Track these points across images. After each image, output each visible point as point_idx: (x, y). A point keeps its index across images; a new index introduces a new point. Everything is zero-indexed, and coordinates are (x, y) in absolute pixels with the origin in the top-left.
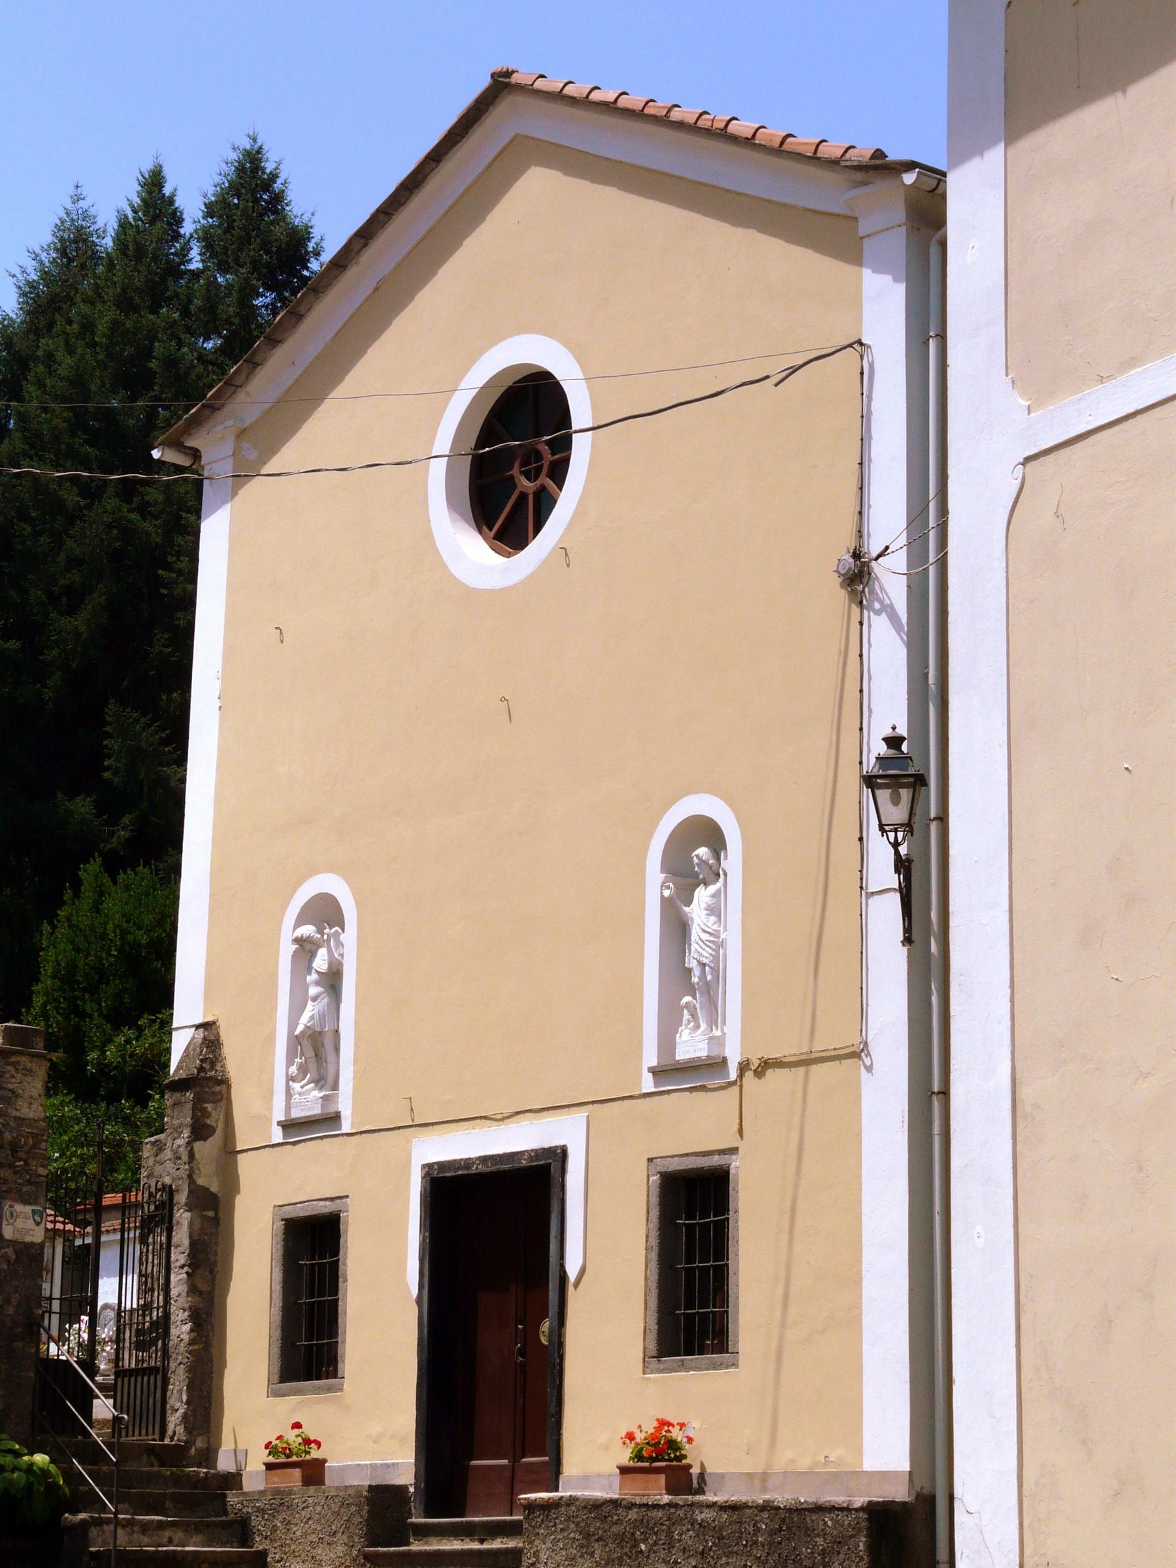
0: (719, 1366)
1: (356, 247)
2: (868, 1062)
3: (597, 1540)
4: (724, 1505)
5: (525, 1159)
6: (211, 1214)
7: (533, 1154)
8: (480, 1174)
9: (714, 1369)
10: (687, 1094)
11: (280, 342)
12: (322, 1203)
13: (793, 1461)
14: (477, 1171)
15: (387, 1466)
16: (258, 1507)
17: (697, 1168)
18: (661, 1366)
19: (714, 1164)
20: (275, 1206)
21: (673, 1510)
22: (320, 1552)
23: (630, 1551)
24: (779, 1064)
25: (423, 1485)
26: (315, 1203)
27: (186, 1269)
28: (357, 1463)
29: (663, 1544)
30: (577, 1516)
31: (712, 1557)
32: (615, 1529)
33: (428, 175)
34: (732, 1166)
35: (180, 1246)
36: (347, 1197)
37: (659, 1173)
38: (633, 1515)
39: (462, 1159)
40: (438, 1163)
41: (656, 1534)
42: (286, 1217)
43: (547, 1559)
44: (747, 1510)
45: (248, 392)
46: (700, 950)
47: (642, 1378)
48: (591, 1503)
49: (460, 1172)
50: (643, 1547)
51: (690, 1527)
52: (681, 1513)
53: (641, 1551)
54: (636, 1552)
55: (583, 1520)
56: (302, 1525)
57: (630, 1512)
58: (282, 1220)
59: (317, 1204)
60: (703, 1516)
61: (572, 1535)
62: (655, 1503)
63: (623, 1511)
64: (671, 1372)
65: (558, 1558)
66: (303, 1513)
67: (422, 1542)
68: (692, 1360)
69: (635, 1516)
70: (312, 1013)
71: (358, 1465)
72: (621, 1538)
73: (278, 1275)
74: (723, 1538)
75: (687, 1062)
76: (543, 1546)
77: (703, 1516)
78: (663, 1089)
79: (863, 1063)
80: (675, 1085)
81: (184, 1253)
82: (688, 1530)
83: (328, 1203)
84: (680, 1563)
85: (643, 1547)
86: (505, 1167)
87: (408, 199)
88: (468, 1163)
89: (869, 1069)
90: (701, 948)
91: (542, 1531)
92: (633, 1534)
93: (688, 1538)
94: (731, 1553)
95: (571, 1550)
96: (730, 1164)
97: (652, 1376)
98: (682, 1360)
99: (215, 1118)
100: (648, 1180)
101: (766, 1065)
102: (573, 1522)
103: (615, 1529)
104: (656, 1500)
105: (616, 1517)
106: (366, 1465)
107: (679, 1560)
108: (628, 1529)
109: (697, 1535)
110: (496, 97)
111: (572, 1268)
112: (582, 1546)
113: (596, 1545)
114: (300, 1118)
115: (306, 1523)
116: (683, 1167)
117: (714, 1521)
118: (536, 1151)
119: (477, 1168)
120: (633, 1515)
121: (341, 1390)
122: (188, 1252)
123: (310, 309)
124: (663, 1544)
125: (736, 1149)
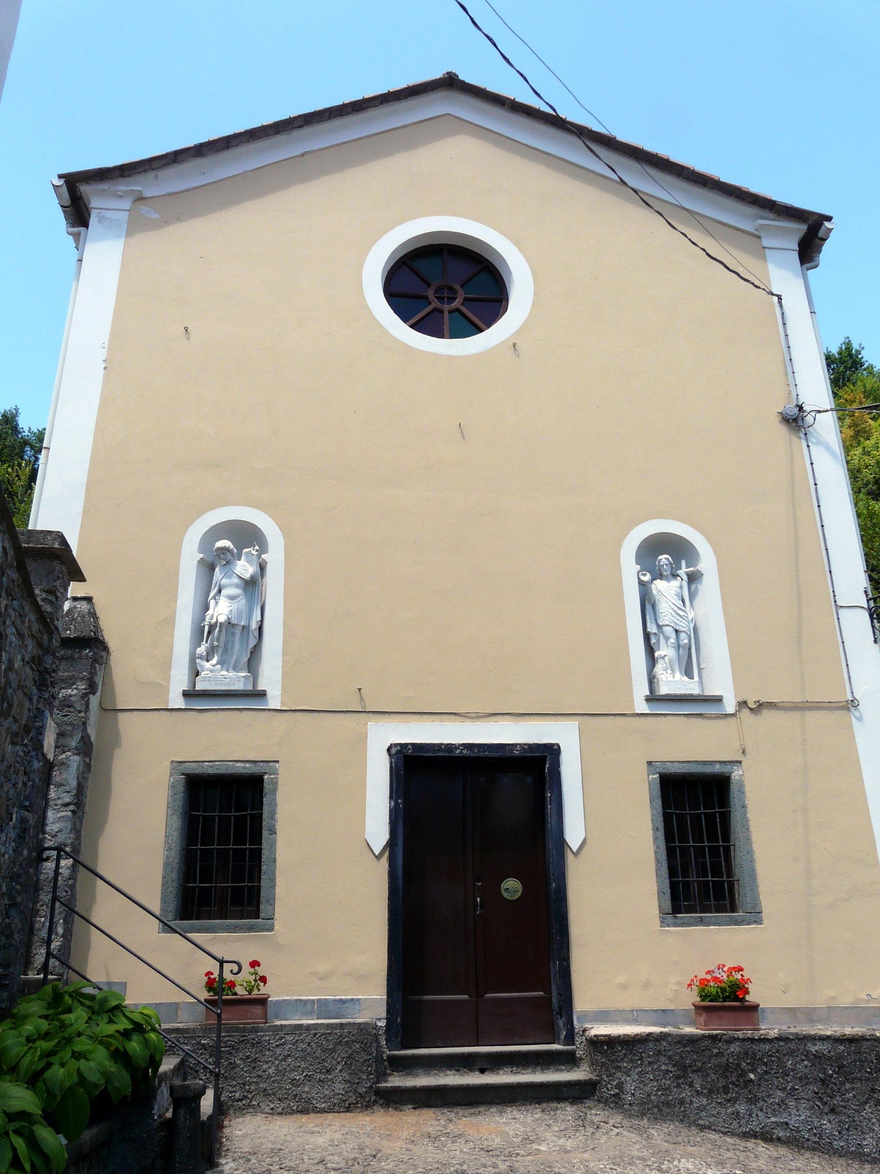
0: (740, 923)
1: (296, 124)
2: (857, 714)
3: (694, 1072)
4: (841, 1038)
5: (517, 750)
6: (87, 760)
7: (526, 747)
8: (463, 757)
9: (736, 924)
10: (684, 719)
11: (202, 155)
12: (242, 765)
13: (835, 998)
14: (460, 755)
15: (343, 1002)
16: (203, 1045)
17: (698, 773)
18: (678, 921)
19: (716, 771)
20: (172, 762)
21: (782, 1044)
22: (306, 1089)
23: (738, 1081)
24: (771, 705)
25: (399, 1020)
26: (231, 763)
27: (72, 807)
28: (296, 998)
29: (775, 1073)
30: (669, 1050)
31: (835, 1084)
32: (714, 1061)
33: (370, 107)
34: (733, 774)
35: (64, 785)
36: (278, 762)
37: (659, 773)
38: (734, 1048)
39: (443, 744)
40: (413, 745)
41: (766, 1064)
42: (187, 772)
43: (634, 1090)
44: (865, 1043)
45: (157, 175)
46: (676, 621)
47: (661, 930)
48: (687, 1038)
49: (440, 754)
50: (752, 1076)
51: (803, 1057)
52: (792, 1046)
53: (751, 1080)
54: (744, 1081)
55: (677, 1053)
56: (277, 1062)
57: (732, 1045)
58: (183, 774)
59: (233, 766)
60: (816, 1048)
61: (663, 1067)
62: (762, 1037)
63: (723, 1045)
64: (691, 927)
65: (647, 1089)
66: (278, 1051)
67: (403, 1073)
68: (711, 917)
69: (738, 1049)
70: (231, 608)
71: (301, 1000)
72: (725, 1070)
73: (176, 823)
74: (843, 1066)
75: (678, 696)
76: (628, 1079)
77: (816, 1048)
78: (663, 712)
79: (855, 716)
80: (671, 711)
81: (69, 792)
82: (803, 1060)
83: (248, 765)
84: (798, 1089)
85: (752, 1076)
86: (496, 755)
87: (349, 114)
88: (450, 747)
89: (860, 719)
90: (678, 620)
91: (625, 1065)
92: (738, 1065)
93: (803, 1067)
94: (854, 1079)
95: (664, 1081)
96: (732, 772)
97: (672, 929)
98: (701, 917)
99: (99, 680)
100: (648, 778)
101: (760, 707)
102: (665, 1056)
103: (714, 1061)
104: (762, 1035)
105: (715, 1051)
106: (313, 1001)
107: (797, 1087)
108: (731, 1061)
109: (813, 1065)
110: (437, 88)
111: (574, 833)
112: (679, 1077)
113: (695, 1076)
114: (210, 690)
115: (284, 1060)
116: (684, 771)
117: (829, 1052)
118: (529, 745)
119: (461, 752)
120: (734, 1048)
121: (271, 929)
122: (75, 791)
123: (236, 146)
124: (775, 1073)
125: (740, 762)
